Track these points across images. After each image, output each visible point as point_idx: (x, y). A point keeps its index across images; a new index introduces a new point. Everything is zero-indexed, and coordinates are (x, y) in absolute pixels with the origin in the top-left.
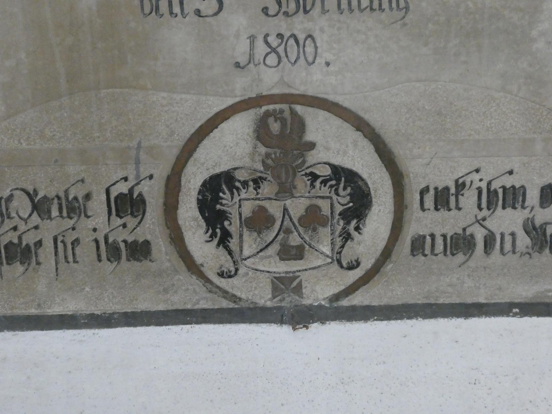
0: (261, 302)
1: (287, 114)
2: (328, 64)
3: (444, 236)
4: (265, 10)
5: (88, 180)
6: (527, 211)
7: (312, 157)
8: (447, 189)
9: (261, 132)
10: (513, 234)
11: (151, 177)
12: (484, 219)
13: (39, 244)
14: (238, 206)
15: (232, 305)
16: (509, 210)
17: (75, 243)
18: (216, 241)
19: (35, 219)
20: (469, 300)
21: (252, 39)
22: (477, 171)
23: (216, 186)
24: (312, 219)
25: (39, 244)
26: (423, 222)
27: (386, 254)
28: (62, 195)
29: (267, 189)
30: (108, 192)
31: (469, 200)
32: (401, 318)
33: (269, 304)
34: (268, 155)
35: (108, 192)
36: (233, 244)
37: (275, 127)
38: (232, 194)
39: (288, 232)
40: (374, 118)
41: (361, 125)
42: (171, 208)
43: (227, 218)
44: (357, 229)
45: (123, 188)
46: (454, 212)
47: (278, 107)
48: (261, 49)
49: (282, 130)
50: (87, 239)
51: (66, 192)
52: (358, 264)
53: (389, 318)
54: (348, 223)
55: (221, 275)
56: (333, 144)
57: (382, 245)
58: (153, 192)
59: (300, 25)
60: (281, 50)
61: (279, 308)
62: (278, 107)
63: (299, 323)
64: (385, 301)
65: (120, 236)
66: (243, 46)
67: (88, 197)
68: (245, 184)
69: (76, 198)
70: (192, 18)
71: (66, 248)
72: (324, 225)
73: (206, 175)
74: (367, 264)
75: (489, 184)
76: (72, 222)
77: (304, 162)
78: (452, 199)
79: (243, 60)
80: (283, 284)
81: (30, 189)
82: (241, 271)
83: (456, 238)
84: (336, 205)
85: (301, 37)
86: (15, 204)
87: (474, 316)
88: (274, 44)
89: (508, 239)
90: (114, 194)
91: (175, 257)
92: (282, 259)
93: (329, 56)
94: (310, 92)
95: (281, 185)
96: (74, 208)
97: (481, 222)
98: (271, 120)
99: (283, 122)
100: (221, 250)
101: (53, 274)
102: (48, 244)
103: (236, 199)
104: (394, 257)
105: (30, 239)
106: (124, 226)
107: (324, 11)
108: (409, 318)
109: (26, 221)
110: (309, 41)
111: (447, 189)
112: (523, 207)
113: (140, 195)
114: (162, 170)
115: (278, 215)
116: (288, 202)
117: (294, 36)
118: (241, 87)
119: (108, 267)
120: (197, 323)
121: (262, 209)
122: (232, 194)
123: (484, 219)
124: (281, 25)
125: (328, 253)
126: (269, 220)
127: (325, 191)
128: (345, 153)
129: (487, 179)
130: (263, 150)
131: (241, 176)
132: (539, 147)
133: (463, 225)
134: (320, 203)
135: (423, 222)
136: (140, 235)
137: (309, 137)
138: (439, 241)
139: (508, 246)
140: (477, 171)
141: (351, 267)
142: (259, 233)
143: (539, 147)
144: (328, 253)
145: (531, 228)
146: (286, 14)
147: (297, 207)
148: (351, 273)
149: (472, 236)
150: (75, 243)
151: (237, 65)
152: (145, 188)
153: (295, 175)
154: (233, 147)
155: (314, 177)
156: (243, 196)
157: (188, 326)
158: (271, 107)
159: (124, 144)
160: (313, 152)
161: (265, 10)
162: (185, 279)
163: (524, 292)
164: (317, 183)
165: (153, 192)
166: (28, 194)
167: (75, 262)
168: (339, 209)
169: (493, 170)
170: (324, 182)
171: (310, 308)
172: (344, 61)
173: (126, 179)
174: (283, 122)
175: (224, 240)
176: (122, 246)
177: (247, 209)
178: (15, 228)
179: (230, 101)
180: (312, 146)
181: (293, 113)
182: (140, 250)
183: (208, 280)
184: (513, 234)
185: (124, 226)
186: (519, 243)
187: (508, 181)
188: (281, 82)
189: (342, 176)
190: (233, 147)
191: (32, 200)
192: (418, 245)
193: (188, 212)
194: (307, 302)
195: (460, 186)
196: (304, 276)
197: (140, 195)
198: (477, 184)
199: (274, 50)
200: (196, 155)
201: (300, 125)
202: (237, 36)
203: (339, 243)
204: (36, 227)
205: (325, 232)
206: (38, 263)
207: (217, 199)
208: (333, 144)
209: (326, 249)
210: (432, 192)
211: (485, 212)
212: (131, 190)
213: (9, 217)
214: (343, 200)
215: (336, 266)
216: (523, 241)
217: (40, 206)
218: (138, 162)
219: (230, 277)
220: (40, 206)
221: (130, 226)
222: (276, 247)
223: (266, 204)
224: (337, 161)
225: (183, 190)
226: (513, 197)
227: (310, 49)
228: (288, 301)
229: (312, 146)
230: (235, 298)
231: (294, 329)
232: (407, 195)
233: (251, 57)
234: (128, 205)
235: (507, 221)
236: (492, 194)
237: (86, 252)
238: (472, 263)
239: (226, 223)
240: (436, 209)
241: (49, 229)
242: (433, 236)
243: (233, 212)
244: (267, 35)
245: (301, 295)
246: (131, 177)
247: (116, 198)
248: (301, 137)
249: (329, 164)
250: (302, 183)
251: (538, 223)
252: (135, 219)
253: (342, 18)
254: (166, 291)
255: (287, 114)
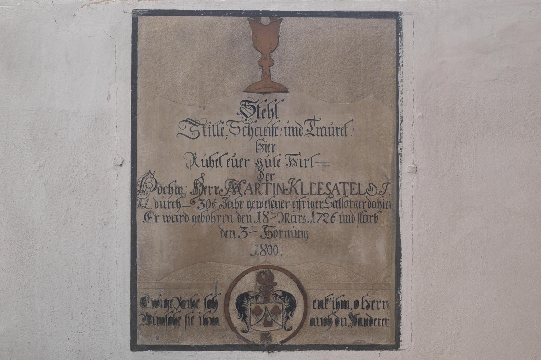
0: (257, 343)
1: (268, 272)
2: (281, 255)
3: (321, 318)
4: (261, 236)
5: (199, 295)
6: (350, 310)
7: (276, 288)
8: (322, 301)
9: (258, 279)
10: (345, 318)
11: (220, 294)
12: (335, 313)
13: (180, 318)
14: (250, 305)
15: (246, 343)
16: (343, 309)
17: (193, 317)
18: (241, 319)
19: (180, 309)
20: (331, 344)
21: (257, 246)
22: (332, 294)
23: (243, 297)
24: (276, 311)
25: (180, 318)
26: (315, 313)
27: (301, 325)
28: (189, 300)
29: (260, 300)
30: (205, 299)
31: (330, 305)
32: (307, 350)
33: (259, 343)
34: (261, 287)
35: (205, 299)
36: (248, 320)
37: (263, 277)
38: (248, 301)
39: (267, 316)
40: (296, 274)
41: (292, 277)
42: (226, 305)
43: (246, 310)
44: (291, 315)
45: (210, 298)
46: (325, 310)
47: (265, 270)
48: (259, 250)
49: (266, 277)
50: (197, 317)
51: (191, 299)
52: (292, 329)
53: (302, 350)
54: (288, 313)
55: (243, 332)
56: (283, 284)
57: (300, 321)
58: (220, 299)
59: (273, 242)
60: (266, 250)
61: (263, 345)
62: (265, 270)
63: (270, 350)
64: (301, 343)
65: (209, 316)
66: (254, 249)
67: (198, 301)
68: (252, 297)
69: (194, 301)
70: (237, 239)
71: (189, 319)
72: (280, 314)
73: (239, 294)
74: (295, 329)
75: (336, 299)
76: (192, 310)
77: (273, 290)
78: (324, 305)
79: (253, 253)
80: (266, 336)
81: (179, 297)
82: (250, 330)
83: (325, 319)
84: (284, 306)
85: (273, 246)
86: (173, 302)
87: (332, 350)
88: (264, 248)
89: (344, 320)
90: (207, 300)
91: (227, 324)
92: (265, 326)
93: (282, 252)
94: (276, 265)
95: (265, 298)
96: (194, 305)
97: (334, 313)
98: (262, 274)
99: (266, 275)
100: (243, 323)
101: (184, 330)
102: (183, 318)
103: (249, 303)
104: (304, 326)
105: (177, 316)
106: (210, 312)
107: (321, 318)
108: (310, 350)
109: (176, 309)
110: (275, 247)
111: (322, 301)
112: (348, 309)
113: (216, 300)
114: (224, 292)
115: (264, 309)
116: (267, 304)
117: (270, 245)
118: (253, 262)
119: (203, 327)
120: (234, 350)
121: (258, 307)
122: (248, 301)
123: (335, 313)
124: (267, 242)
125: (281, 324)
126: (261, 311)
127: (280, 301)
128: (287, 287)
129: (336, 297)
130: (259, 285)
131: (251, 294)
132: (353, 286)
133: (328, 315)
134: (278, 305)
135: (315, 313)
136: (215, 316)
137: (275, 281)
138: (320, 320)
139: (344, 323)
140: (332, 294)
141: (290, 329)
142: (257, 316)
143: (353, 286)
144: (281, 324)
145: (351, 316)
146: (268, 238)
147: (270, 306)
148: (289, 332)
149: (331, 319)
150: (193, 317)
151: (251, 255)
152: (218, 298)
153: (270, 294)
154: (249, 283)
155: (277, 295)
156: (252, 302)
157: (230, 351)
158: (262, 270)
159: (212, 282)
160: (276, 286)
161: (261, 236)
162: (230, 333)
163: (350, 341)
164: (278, 298)
165: (220, 299)
166: (178, 299)
167: (192, 325)
168: (285, 307)
169: (337, 295)
170: (280, 297)
171: (274, 345)
172: (288, 256)
173: (212, 294)
174: (266, 275)
175: (244, 318)
176: (209, 319)
177: (253, 306)
178: (173, 312)
179: (248, 268)
180: (276, 284)
181: (270, 272)
182: (215, 321)
183: (238, 333)
184: (345, 318)
185: (210, 312)
186: (347, 322)
187: (343, 299)
188: (266, 261)
189: (286, 295)
190: (249, 283)
191: (179, 301)
192: (312, 322)
193: (232, 307)
194: (273, 343)
195: (327, 300)
196: (272, 333)
197: (216, 300)
198: (332, 299)
199: (264, 250)
200: (236, 286)
201: (272, 276)
202: (252, 245)
203: (285, 321)
204: (180, 312)
205: (280, 317)
206: (179, 325)
207: (242, 303)
208: (283, 284)
209: (280, 323)
210: (317, 302)
211: (335, 310)
212: (213, 299)
213: (171, 308)
214: (286, 305)
215: (283, 329)
216: (349, 321)
217: (182, 304)
218: (216, 289)
219: (246, 332)
220: (182, 304)
221: (212, 312)
222: (262, 322)
223: (259, 305)
224: (284, 290)
225: (231, 299)
226: (345, 305)
227: (276, 250)
228: (266, 343)
229: (276, 284)
230: (247, 341)
231: (268, 353)
232: (309, 303)
233: (256, 252)
234: (212, 304)
235: (343, 313)
236: (338, 303)
237: (196, 321)
238: (331, 329)
239: (245, 312)
240: (319, 308)
241: (187, 311)
242: (317, 318)
243: (248, 307)
244: (261, 245)
245: (271, 340)
246: (214, 294)
247: (169, 318)
248: (272, 281)
249: (282, 291)
250: (272, 298)
251: (354, 314)
252: (275, 275)
253: (287, 240)
254: (223, 337)
255: (268, 272)
